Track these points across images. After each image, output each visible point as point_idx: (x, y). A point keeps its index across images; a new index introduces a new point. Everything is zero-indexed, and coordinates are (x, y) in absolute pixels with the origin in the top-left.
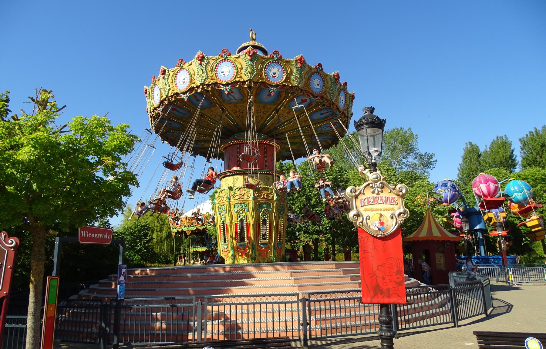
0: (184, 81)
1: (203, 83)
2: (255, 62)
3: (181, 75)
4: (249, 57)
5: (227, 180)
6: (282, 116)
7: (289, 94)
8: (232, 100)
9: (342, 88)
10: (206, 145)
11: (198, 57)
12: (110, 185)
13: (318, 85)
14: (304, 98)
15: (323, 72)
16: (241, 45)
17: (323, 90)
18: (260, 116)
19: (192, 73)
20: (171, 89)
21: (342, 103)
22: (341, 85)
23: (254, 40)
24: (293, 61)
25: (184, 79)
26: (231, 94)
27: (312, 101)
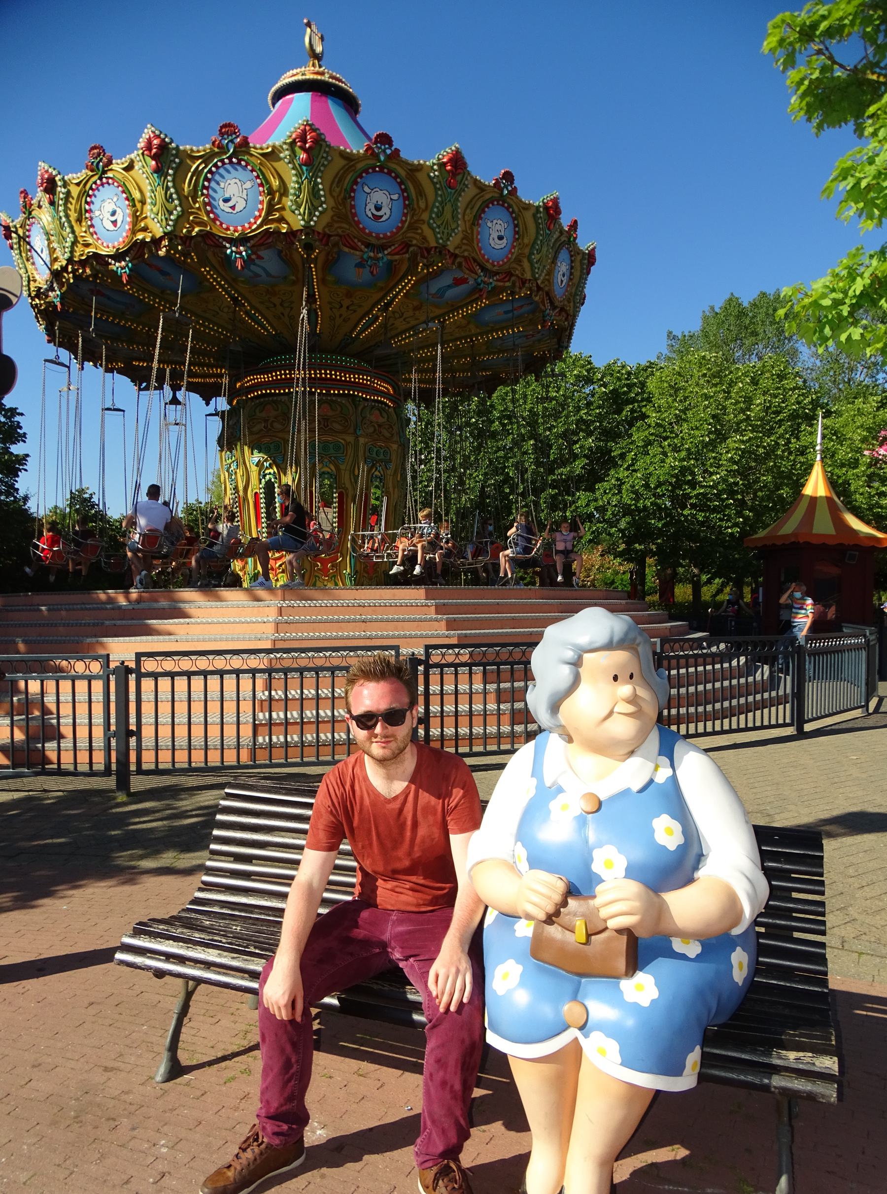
0: (113, 219)
2: (321, 213)
3: (103, 201)
4: (303, 156)
6: (400, 317)
7: (418, 265)
9: (563, 239)
11: (149, 146)
13: (500, 238)
14: (459, 275)
15: (517, 198)
16: (277, 83)
17: (512, 254)
19: (137, 195)
21: (562, 281)
22: (562, 232)
23: (317, 57)
24: (432, 167)
25: (114, 213)
26: (257, 261)
27: (482, 286)
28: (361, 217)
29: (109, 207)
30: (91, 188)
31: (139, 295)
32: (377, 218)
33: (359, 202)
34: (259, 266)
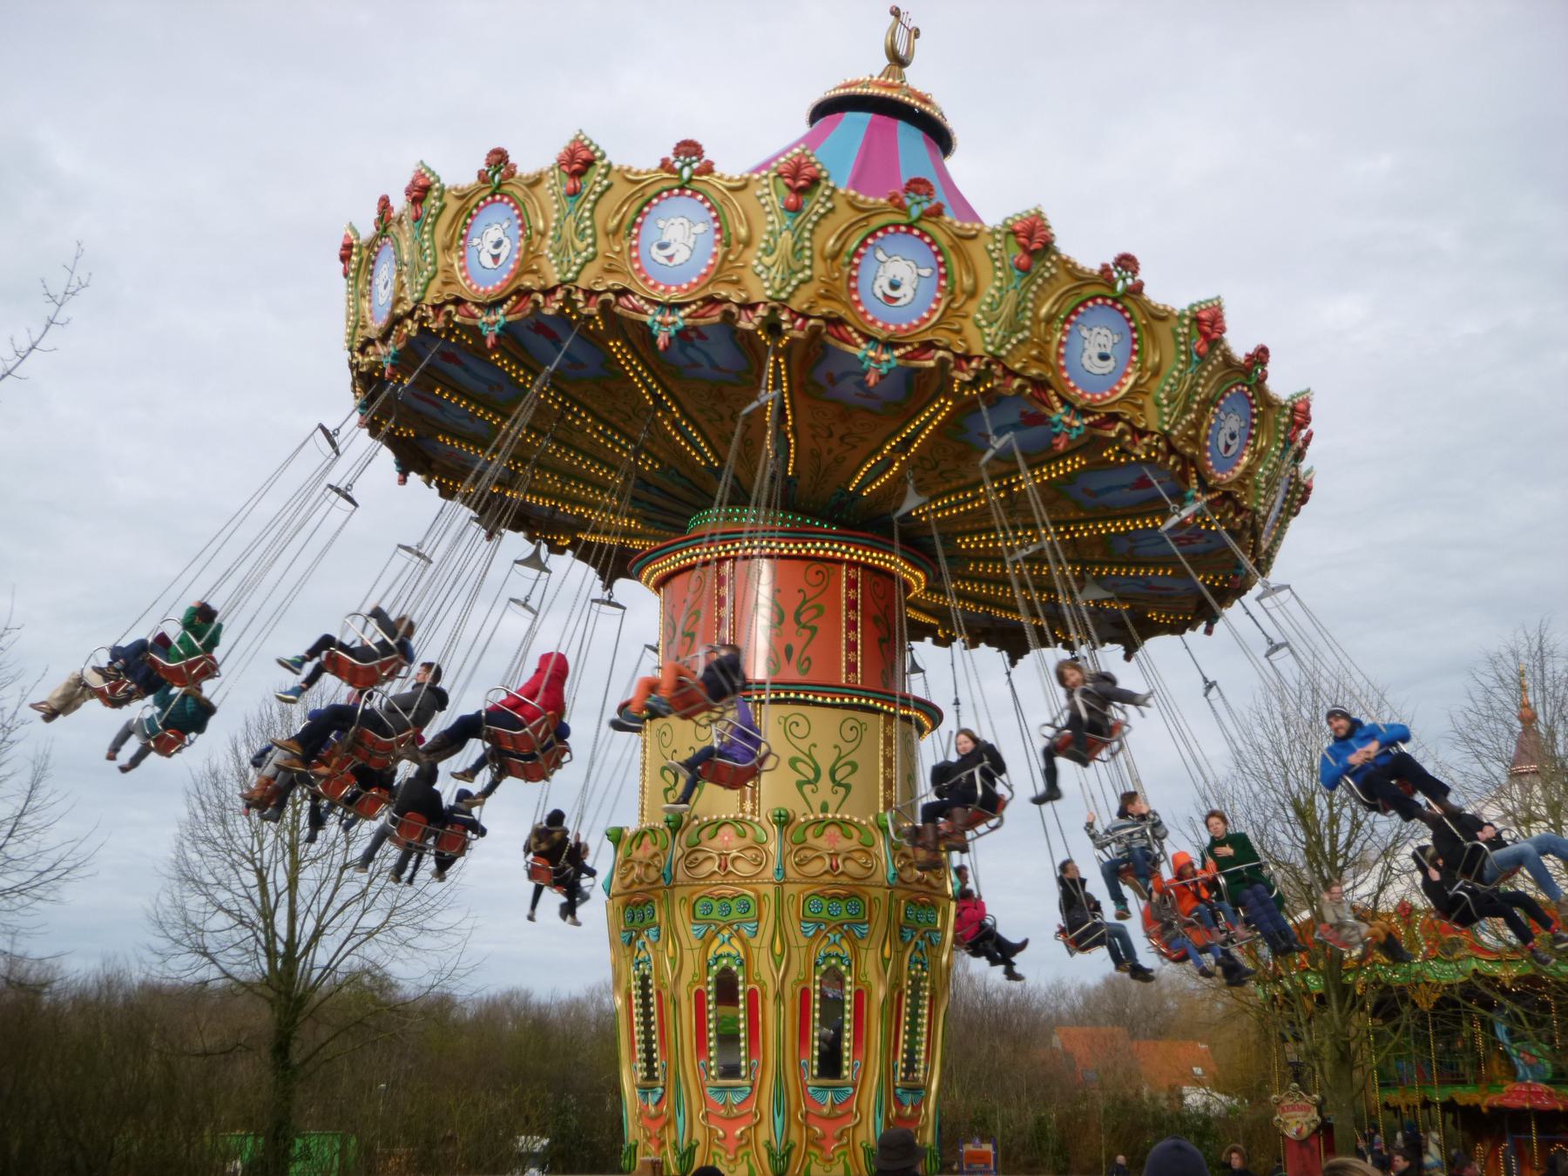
0: (495, 252)
1: (573, 281)
3: (489, 225)
5: (666, 729)
6: (933, 469)
8: (701, 366)
10: (752, 504)
12: (727, 658)
13: (1104, 357)
18: (830, 451)
20: (440, 277)
21: (1228, 447)
25: (498, 244)
26: (697, 342)
28: (863, 294)
29: (494, 234)
30: (477, 206)
31: (519, 376)
32: (890, 300)
33: (865, 273)
34: (698, 349)
